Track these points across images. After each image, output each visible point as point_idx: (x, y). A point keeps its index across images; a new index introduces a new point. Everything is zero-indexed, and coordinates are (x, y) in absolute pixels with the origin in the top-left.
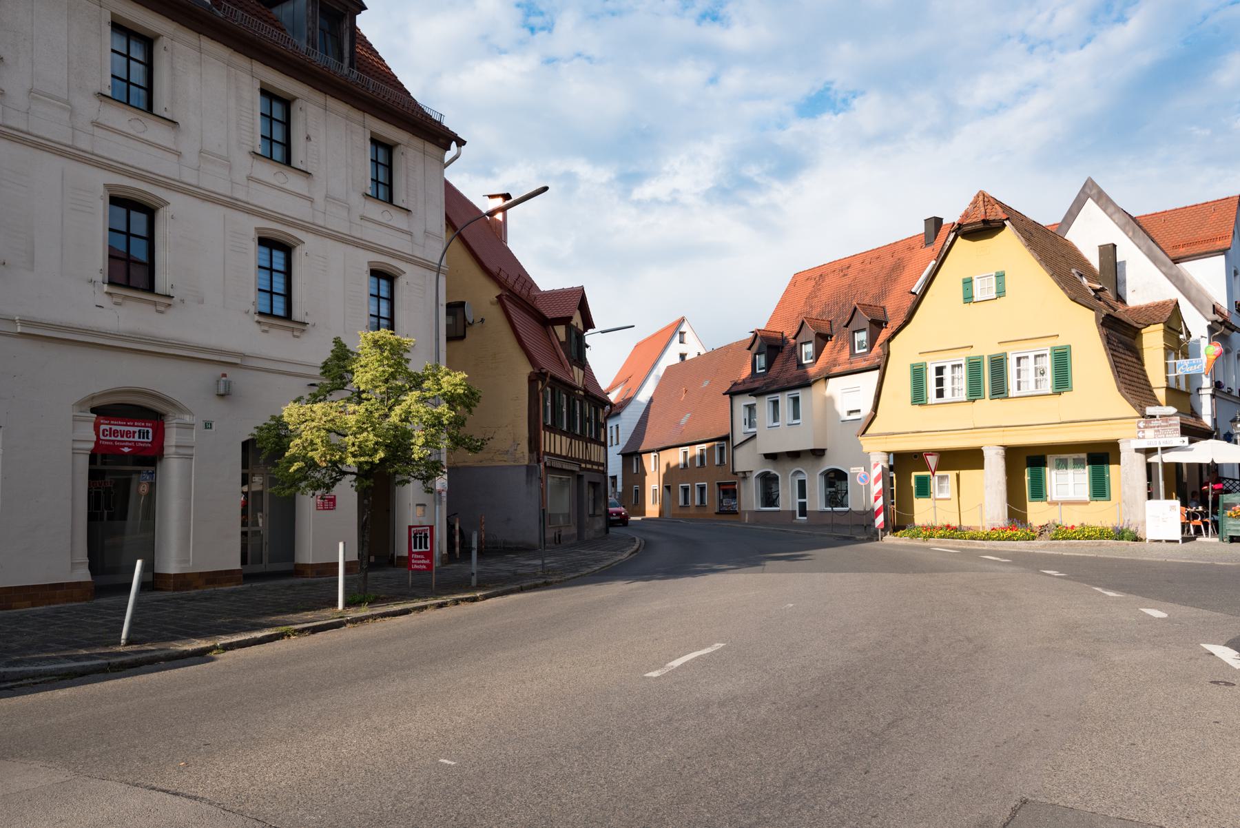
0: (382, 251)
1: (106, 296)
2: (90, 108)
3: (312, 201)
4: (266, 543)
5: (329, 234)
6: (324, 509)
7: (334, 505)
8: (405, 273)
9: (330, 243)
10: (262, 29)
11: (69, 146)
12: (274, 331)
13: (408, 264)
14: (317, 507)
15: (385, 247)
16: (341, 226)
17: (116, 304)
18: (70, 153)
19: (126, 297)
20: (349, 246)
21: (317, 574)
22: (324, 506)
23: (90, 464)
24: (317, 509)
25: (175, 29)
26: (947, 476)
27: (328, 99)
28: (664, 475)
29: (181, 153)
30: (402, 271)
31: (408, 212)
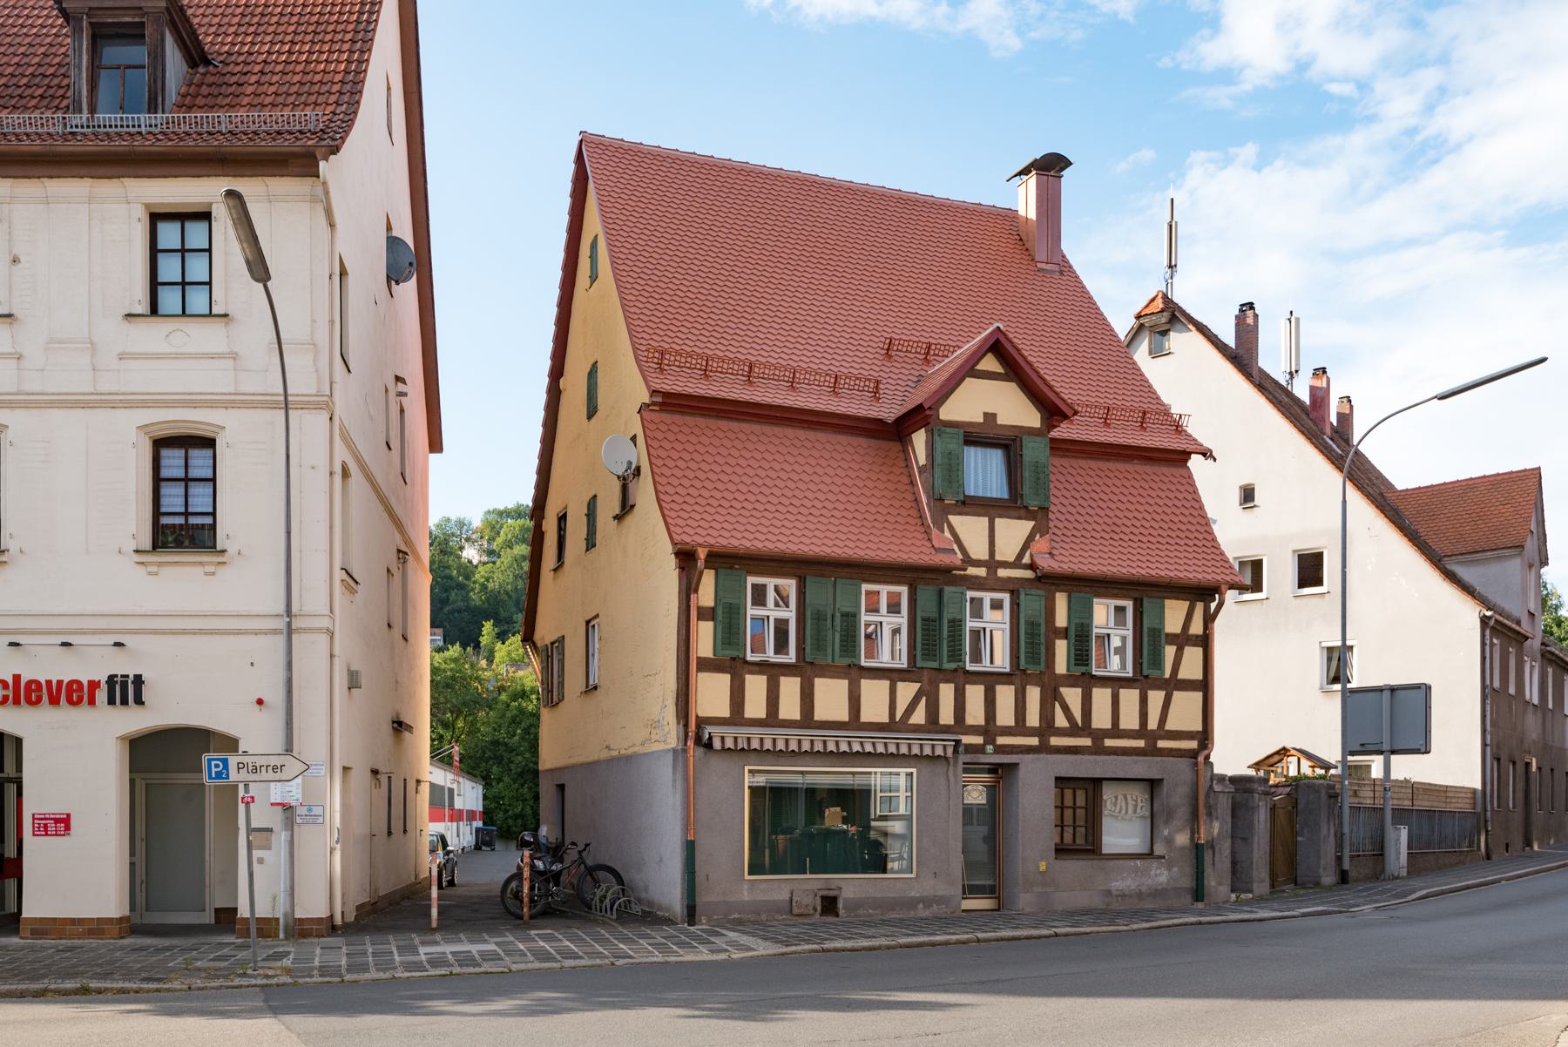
0: (165, 402)
1: (137, 566)
2: (118, 336)
3: (235, 359)
4: (142, 882)
5: (52, 402)
6: (47, 835)
7: (68, 828)
8: (7, 427)
9: (57, 415)
10: (202, 124)
11: (92, 394)
12: (167, 572)
13: (230, 410)
14: (34, 831)
15: (84, 394)
16: (79, 383)
17: (150, 573)
18: (19, 402)
19: (160, 564)
20: (96, 410)
21: (31, 934)
22: (46, 830)
23: (130, 772)
24: (34, 835)
25: (91, 187)
26: (1016, 765)
27: (46, 184)
28: (1314, 784)
29: (236, 354)
30: (219, 427)
31: (9, 320)
